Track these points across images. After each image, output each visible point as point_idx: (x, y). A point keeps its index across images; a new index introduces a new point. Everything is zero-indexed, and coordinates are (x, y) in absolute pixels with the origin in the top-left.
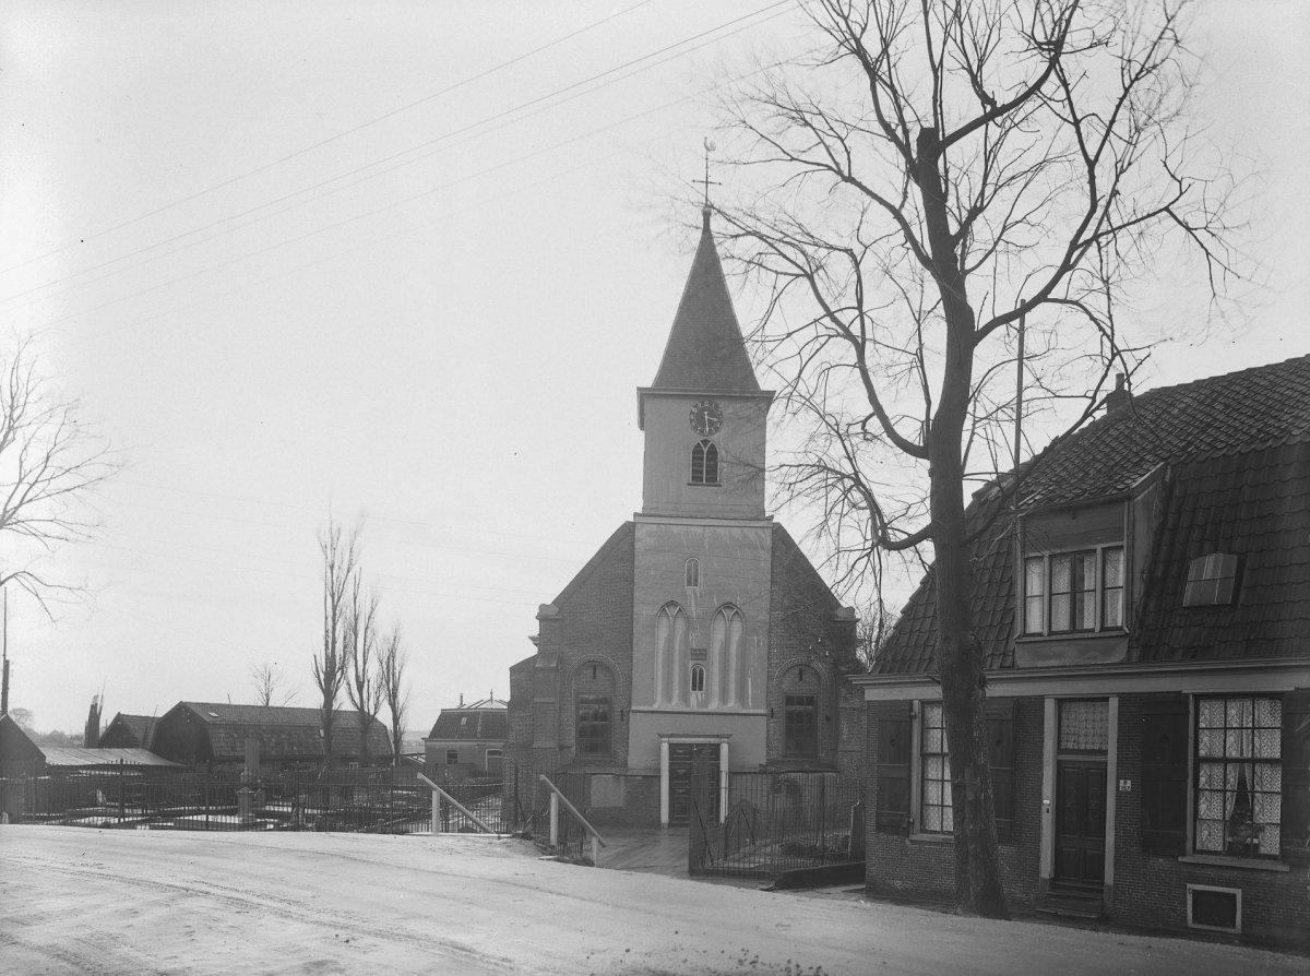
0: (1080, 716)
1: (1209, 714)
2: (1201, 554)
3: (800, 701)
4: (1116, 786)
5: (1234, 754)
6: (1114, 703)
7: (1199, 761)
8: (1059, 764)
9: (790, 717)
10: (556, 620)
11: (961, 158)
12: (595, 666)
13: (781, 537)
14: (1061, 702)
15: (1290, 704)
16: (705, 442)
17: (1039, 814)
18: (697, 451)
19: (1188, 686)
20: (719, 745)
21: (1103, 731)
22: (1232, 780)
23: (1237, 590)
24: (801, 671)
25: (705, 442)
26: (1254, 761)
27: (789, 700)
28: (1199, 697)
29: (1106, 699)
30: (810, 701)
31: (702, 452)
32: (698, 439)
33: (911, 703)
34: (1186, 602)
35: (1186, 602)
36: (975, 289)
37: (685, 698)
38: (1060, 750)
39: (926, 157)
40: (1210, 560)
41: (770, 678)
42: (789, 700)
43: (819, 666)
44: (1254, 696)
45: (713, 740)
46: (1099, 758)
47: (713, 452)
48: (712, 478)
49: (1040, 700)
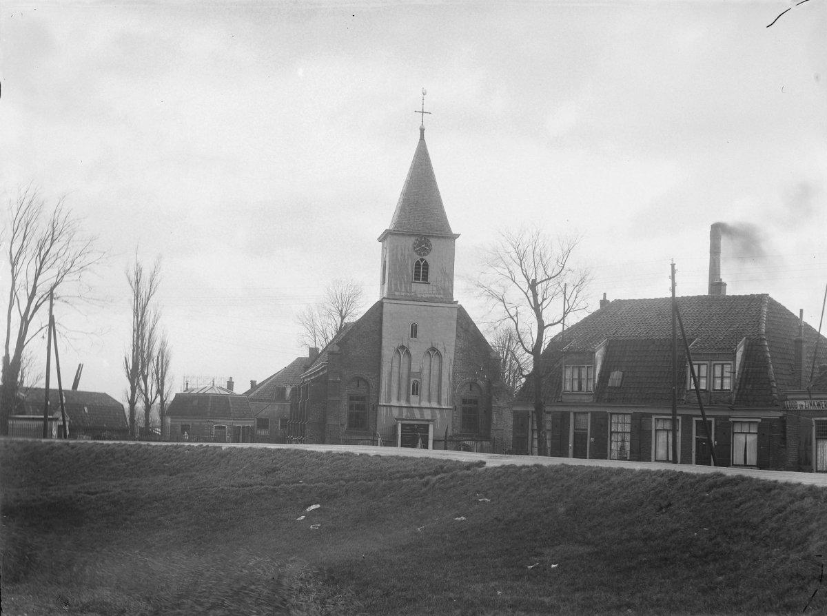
0: (582, 417)
1: (614, 419)
2: (614, 371)
3: (470, 402)
4: (590, 440)
5: (621, 431)
6: (589, 414)
7: (611, 433)
8: (575, 434)
9: (464, 410)
10: (337, 354)
11: (539, 288)
12: (359, 380)
13: (461, 311)
14: (575, 413)
15: (6, 433)
16: (422, 260)
17: (568, 450)
18: (418, 264)
19: (609, 411)
20: (428, 425)
21: (587, 422)
22: (620, 438)
23: (621, 383)
24: (471, 386)
25: (422, 260)
26: (625, 433)
27: (464, 401)
28: (611, 414)
29: (587, 413)
30: (476, 402)
31: (420, 265)
32: (419, 258)
33: (528, 412)
34: (610, 385)
35: (610, 385)
36: (544, 314)
37: (408, 400)
38: (575, 429)
39: (533, 286)
40: (616, 373)
41: (454, 389)
42: (464, 401)
43: (481, 383)
44: (625, 414)
45: (426, 423)
46: (815, 470)
47: (426, 265)
48: (425, 278)
49: (568, 413)
